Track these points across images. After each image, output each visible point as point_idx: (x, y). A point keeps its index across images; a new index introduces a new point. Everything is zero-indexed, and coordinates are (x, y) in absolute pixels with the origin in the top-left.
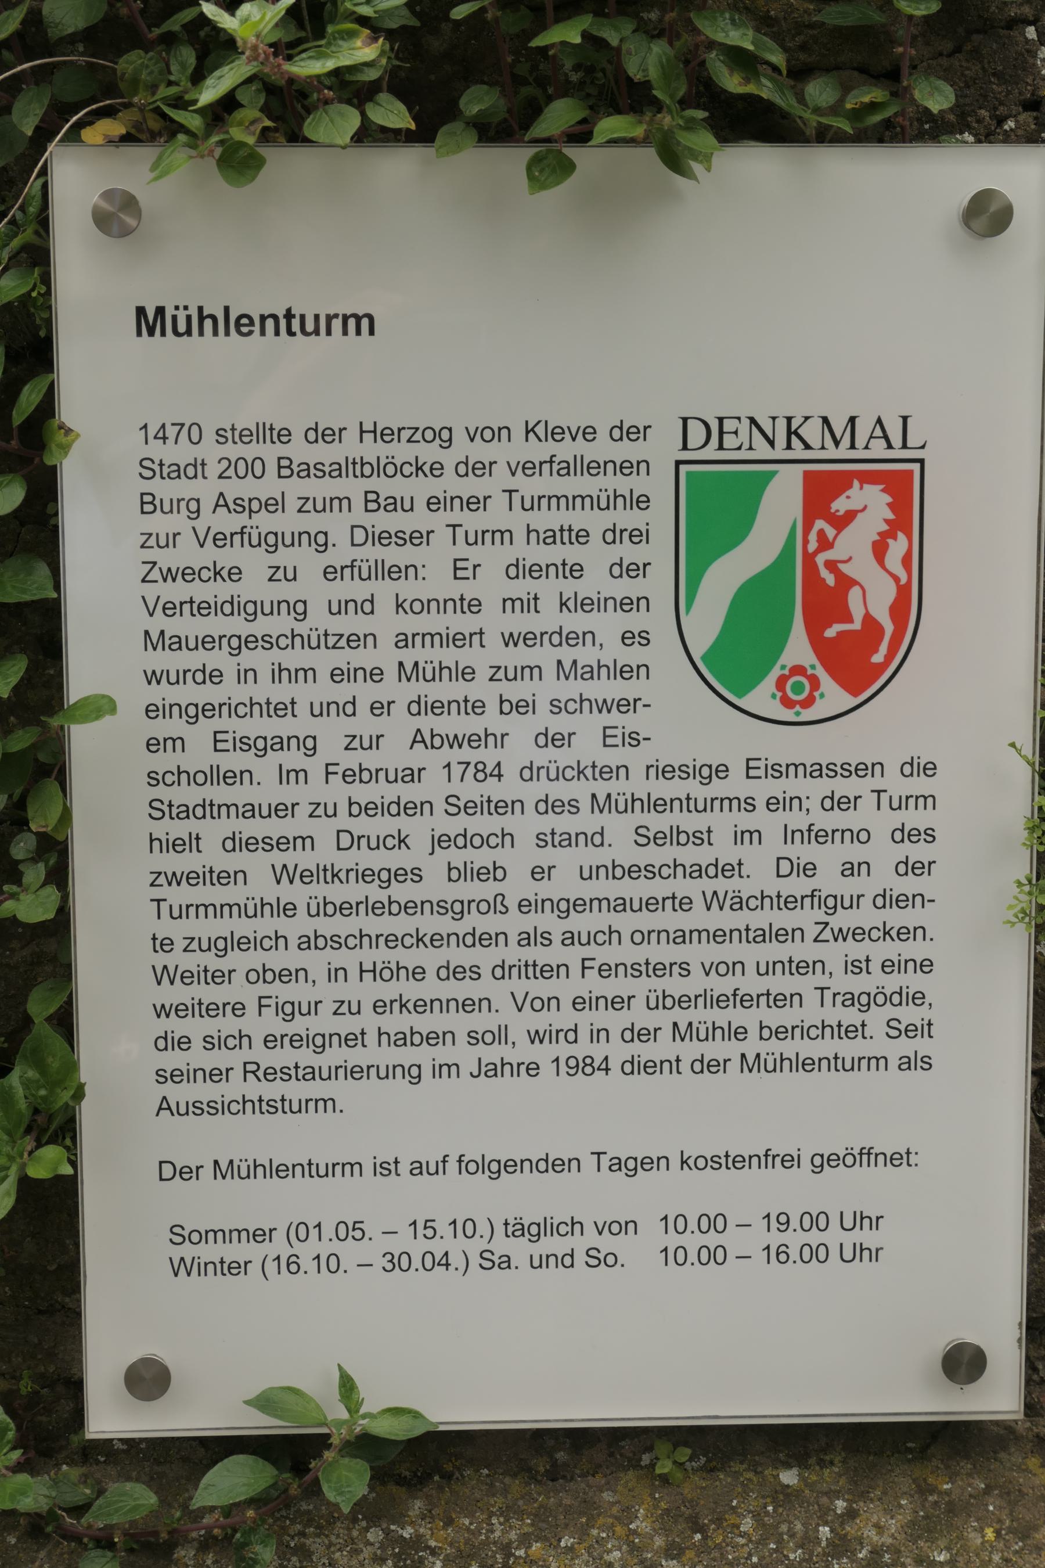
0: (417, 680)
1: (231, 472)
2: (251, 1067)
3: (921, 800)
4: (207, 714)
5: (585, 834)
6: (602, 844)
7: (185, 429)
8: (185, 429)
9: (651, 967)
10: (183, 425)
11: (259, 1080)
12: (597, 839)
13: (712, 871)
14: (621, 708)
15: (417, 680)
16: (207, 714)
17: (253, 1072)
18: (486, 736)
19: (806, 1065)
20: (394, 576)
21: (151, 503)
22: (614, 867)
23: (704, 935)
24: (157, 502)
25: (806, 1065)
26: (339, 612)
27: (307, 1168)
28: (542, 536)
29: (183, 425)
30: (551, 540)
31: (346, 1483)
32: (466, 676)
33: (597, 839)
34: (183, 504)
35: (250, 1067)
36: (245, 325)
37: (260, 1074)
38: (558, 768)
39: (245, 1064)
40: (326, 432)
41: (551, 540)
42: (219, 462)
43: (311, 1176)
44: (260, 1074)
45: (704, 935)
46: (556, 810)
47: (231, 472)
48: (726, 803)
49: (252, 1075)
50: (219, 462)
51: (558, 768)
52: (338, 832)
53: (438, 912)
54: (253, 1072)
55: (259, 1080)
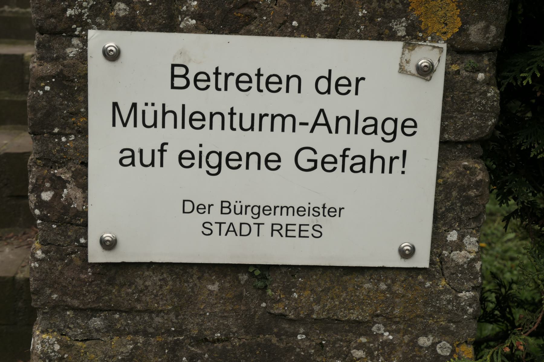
0: (135, 125)
2: (276, 227)
3: (285, 210)
4: (266, 212)
9: (326, 210)
14: (200, 210)
15: (135, 125)
16: (266, 212)
17: (278, 231)
20: (301, 213)
21: (228, 207)
23: (291, 210)
24: (232, 207)
27: (227, 118)
31: (441, 181)
32: (300, 213)
34: (249, 209)
35: (276, 227)
37: (283, 232)
39: (273, 225)
40: (200, 207)
43: (233, 129)
45: (291, 210)
48: (285, 210)
49: (277, 232)
52: (184, 201)
53: (313, 214)
54: (278, 231)
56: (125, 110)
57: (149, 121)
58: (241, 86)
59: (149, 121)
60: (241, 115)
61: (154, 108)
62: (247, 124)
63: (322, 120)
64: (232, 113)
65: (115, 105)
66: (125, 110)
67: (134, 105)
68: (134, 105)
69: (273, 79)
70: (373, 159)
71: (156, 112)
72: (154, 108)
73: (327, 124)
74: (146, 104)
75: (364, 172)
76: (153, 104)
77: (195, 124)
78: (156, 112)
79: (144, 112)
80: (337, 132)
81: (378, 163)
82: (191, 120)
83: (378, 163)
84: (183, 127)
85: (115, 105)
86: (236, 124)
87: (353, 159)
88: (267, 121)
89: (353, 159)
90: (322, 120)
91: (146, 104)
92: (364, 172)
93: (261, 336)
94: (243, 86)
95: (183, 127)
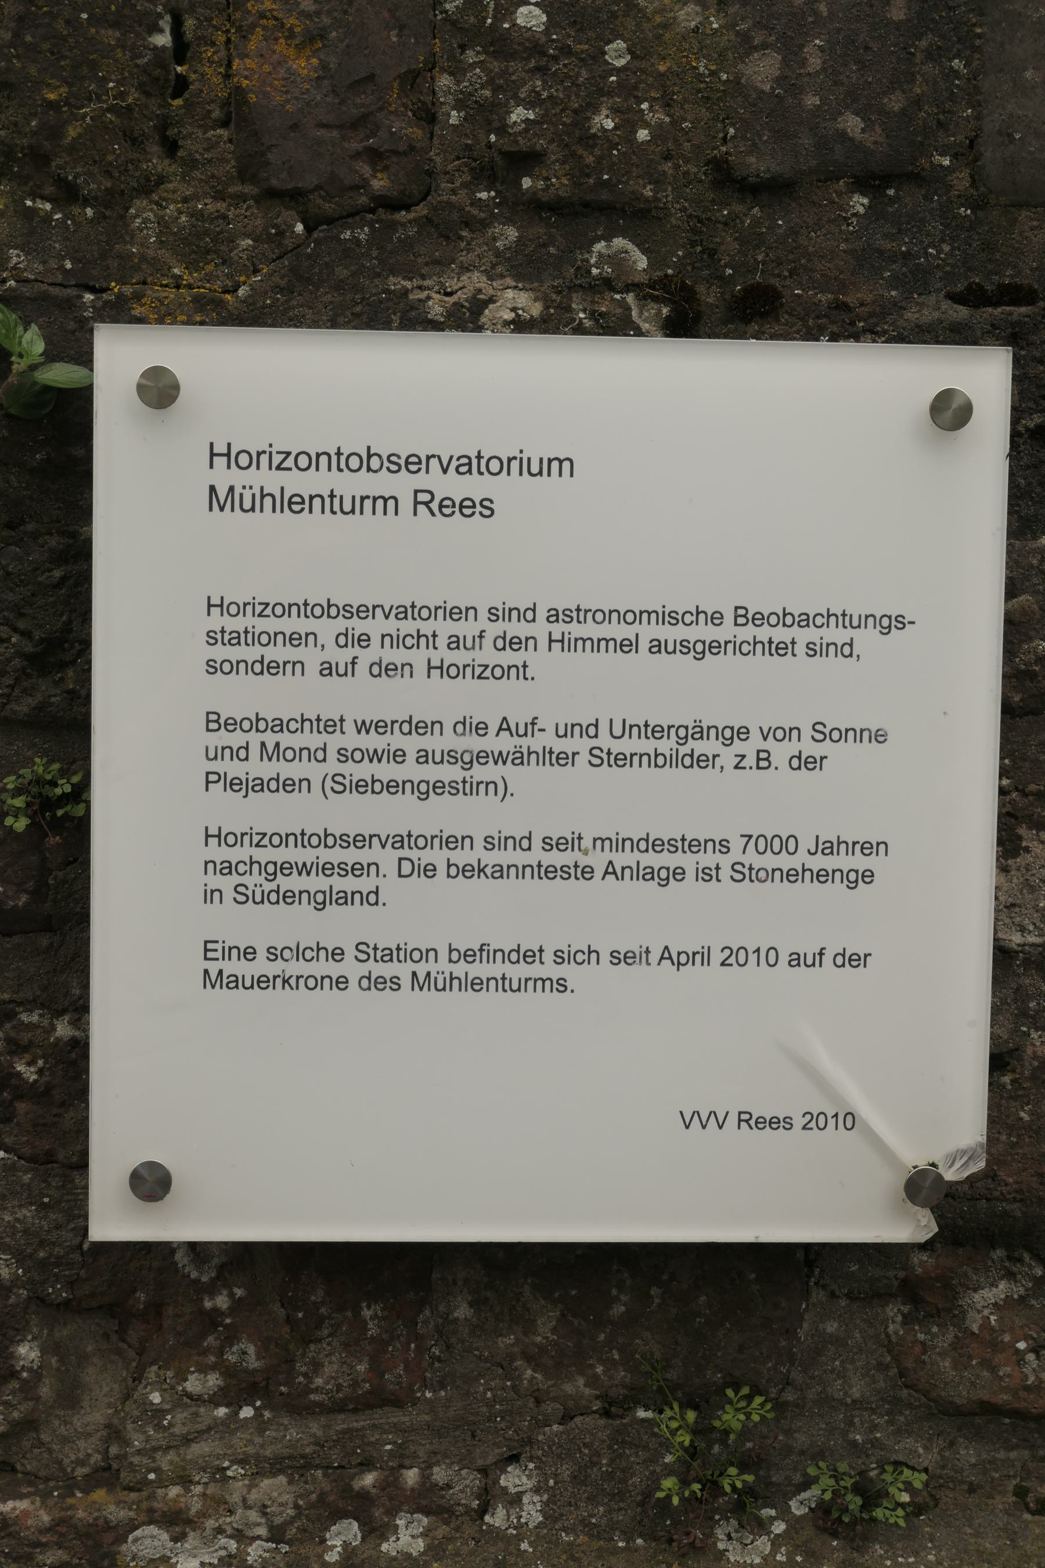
0: (233, 510)
1: (813, 1124)
5: (514, 838)
6: (377, 903)
7: (753, 841)
8: (753, 841)
10: (750, 837)
11: (433, 514)
12: (372, 898)
13: (273, 785)
15: (233, 510)
18: (804, 871)
19: (295, 504)
22: (656, 756)
25: (295, 504)
26: (353, 511)
28: (219, 867)
29: (750, 837)
30: (466, 468)
33: (372, 898)
36: (448, 507)
37: (435, 506)
38: (263, 891)
41: (466, 468)
42: (722, 951)
44: (435, 506)
46: (715, 621)
47: (813, 1124)
50: (722, 951)
51: (263, 891)
55: (433, 514)
56: (222, 493)
57: (247, 505)
58: (865, 851)
59: (247, 505)
60: (341, 497)
61: (252, 491)
62: (347, 507)
63: (666, 955)
64: (332, 496)
65: (212, 489)
66: (222, 493)
67: (231, 489)
68: (231, 489)
69: (562, 756)
70: (839, 844)
71: (254, 495)
72: (252, 491)
73: (670, 958)
74: (244, 487)
75: (471, 474)
76: (251, 488)
77: (294, 507)
78: (254, 495)
79: (241, 495)
80: (623, 879)
81: (843, 847)
82: (290, 503)
83: (843, 847)
84: (282, 511)
85: (212, 489)
86: (336, 508)
87: (230, 634)
88: (368, 504)
89: (230, 634)
90: (666, 955)
91: (244, 487)
92: (471, 474)
93: (963, 209)
94: (867, 852)
95: (282, 511)
